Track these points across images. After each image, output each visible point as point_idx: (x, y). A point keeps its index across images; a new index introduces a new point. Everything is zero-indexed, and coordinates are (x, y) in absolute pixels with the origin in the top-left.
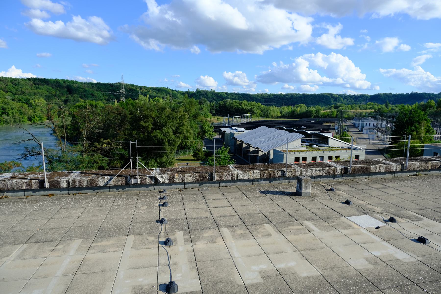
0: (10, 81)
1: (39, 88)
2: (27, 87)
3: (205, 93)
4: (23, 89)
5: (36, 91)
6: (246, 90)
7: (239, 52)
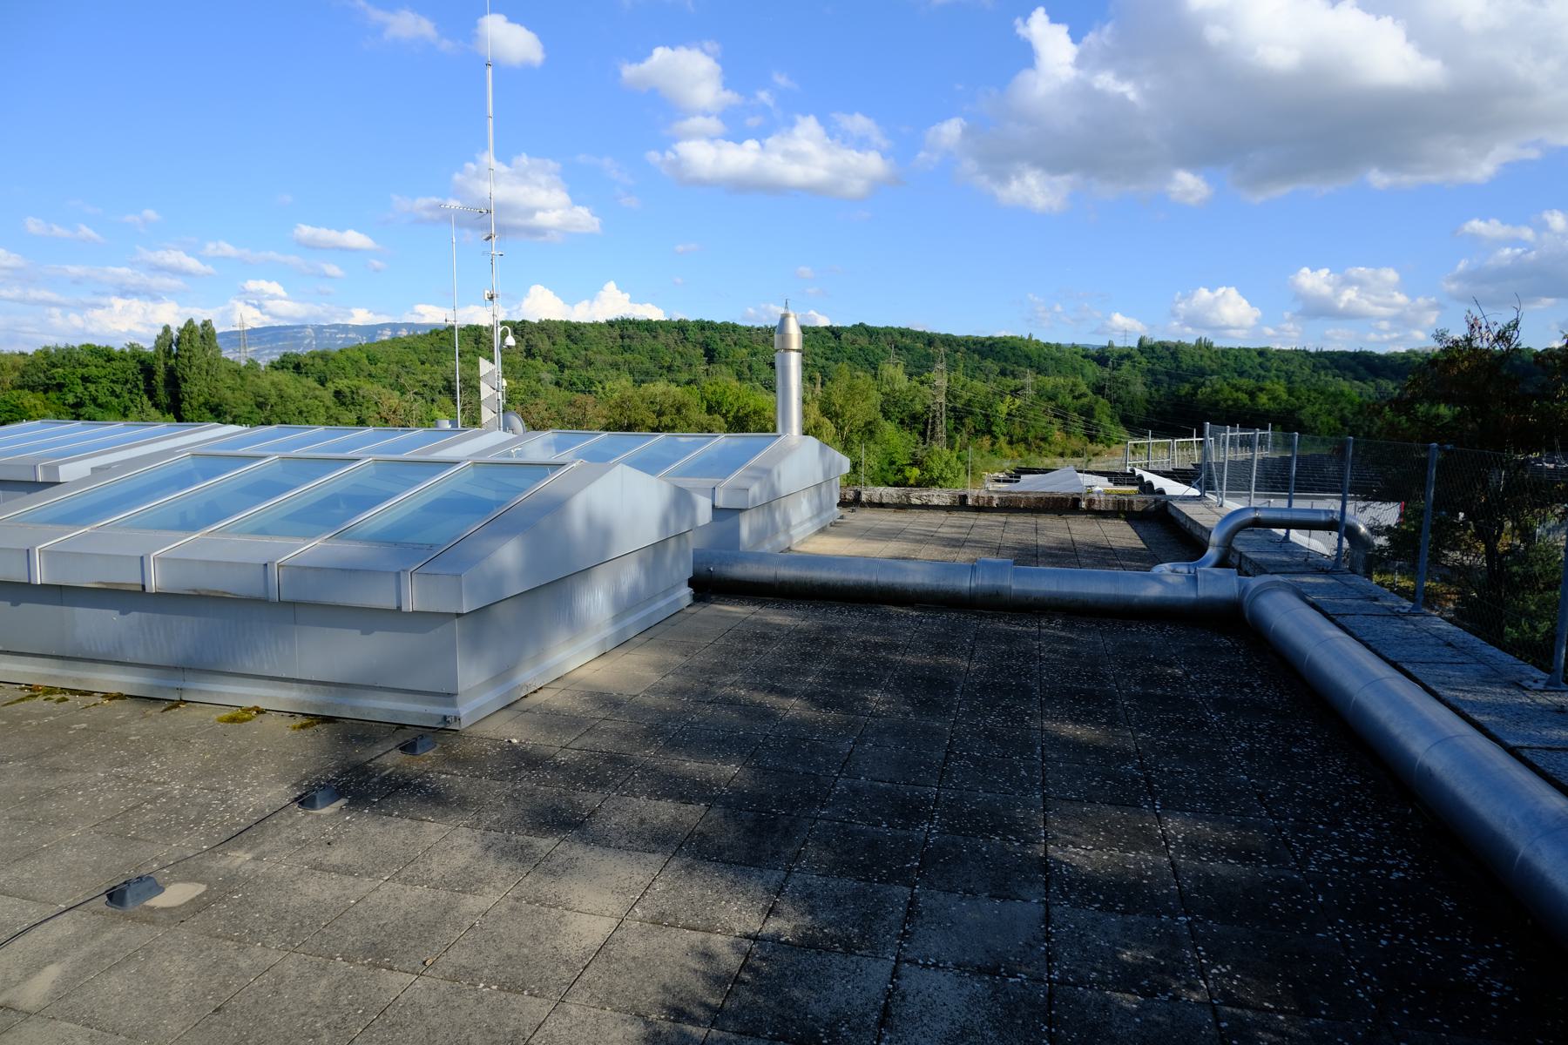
0: (566, 331)
1: (630, 349)
2: (602, 348)
3: (1172, 354)
4: (589, 353)
5: (619, 359)
6: (1386, 337)
7: (1378, 178)
